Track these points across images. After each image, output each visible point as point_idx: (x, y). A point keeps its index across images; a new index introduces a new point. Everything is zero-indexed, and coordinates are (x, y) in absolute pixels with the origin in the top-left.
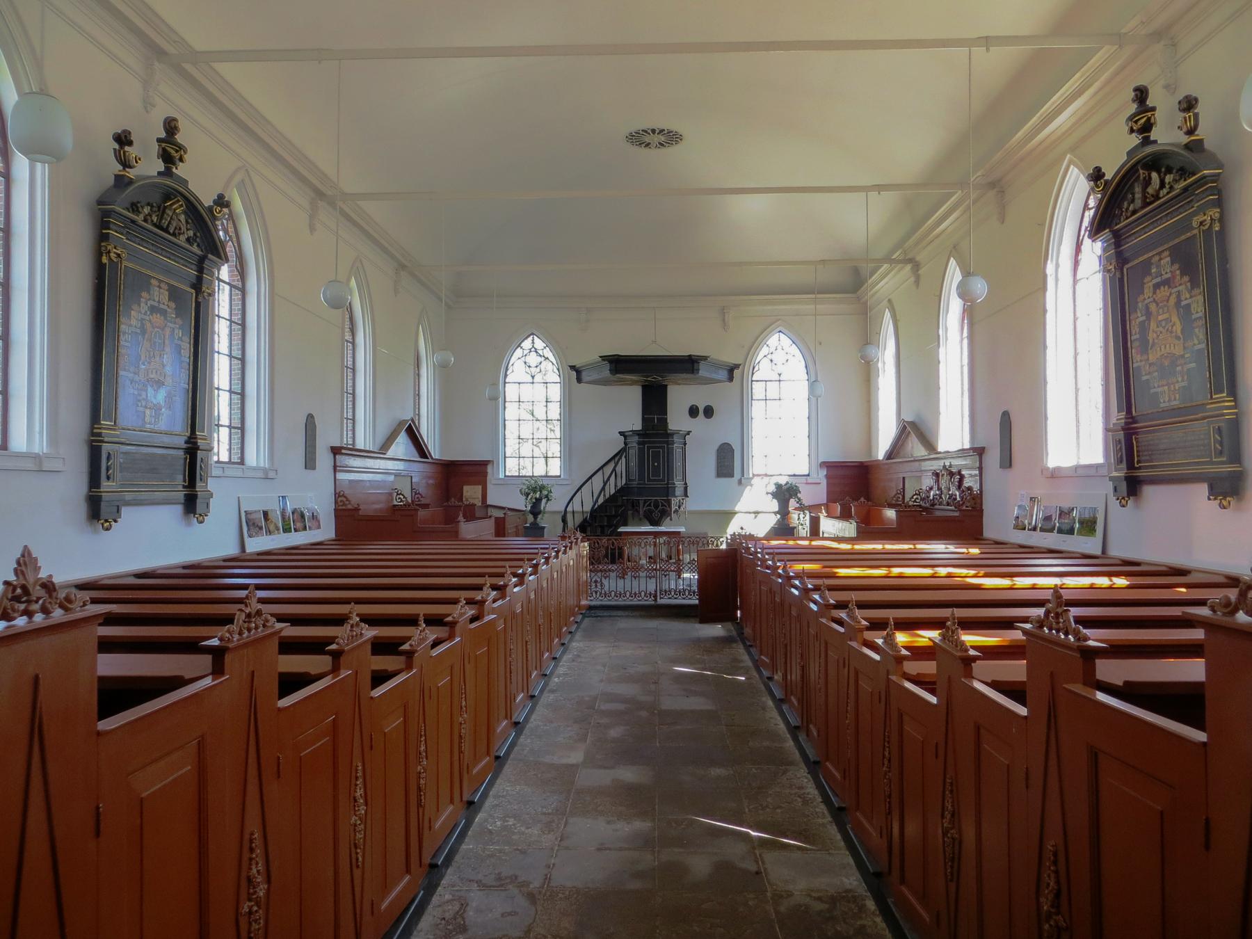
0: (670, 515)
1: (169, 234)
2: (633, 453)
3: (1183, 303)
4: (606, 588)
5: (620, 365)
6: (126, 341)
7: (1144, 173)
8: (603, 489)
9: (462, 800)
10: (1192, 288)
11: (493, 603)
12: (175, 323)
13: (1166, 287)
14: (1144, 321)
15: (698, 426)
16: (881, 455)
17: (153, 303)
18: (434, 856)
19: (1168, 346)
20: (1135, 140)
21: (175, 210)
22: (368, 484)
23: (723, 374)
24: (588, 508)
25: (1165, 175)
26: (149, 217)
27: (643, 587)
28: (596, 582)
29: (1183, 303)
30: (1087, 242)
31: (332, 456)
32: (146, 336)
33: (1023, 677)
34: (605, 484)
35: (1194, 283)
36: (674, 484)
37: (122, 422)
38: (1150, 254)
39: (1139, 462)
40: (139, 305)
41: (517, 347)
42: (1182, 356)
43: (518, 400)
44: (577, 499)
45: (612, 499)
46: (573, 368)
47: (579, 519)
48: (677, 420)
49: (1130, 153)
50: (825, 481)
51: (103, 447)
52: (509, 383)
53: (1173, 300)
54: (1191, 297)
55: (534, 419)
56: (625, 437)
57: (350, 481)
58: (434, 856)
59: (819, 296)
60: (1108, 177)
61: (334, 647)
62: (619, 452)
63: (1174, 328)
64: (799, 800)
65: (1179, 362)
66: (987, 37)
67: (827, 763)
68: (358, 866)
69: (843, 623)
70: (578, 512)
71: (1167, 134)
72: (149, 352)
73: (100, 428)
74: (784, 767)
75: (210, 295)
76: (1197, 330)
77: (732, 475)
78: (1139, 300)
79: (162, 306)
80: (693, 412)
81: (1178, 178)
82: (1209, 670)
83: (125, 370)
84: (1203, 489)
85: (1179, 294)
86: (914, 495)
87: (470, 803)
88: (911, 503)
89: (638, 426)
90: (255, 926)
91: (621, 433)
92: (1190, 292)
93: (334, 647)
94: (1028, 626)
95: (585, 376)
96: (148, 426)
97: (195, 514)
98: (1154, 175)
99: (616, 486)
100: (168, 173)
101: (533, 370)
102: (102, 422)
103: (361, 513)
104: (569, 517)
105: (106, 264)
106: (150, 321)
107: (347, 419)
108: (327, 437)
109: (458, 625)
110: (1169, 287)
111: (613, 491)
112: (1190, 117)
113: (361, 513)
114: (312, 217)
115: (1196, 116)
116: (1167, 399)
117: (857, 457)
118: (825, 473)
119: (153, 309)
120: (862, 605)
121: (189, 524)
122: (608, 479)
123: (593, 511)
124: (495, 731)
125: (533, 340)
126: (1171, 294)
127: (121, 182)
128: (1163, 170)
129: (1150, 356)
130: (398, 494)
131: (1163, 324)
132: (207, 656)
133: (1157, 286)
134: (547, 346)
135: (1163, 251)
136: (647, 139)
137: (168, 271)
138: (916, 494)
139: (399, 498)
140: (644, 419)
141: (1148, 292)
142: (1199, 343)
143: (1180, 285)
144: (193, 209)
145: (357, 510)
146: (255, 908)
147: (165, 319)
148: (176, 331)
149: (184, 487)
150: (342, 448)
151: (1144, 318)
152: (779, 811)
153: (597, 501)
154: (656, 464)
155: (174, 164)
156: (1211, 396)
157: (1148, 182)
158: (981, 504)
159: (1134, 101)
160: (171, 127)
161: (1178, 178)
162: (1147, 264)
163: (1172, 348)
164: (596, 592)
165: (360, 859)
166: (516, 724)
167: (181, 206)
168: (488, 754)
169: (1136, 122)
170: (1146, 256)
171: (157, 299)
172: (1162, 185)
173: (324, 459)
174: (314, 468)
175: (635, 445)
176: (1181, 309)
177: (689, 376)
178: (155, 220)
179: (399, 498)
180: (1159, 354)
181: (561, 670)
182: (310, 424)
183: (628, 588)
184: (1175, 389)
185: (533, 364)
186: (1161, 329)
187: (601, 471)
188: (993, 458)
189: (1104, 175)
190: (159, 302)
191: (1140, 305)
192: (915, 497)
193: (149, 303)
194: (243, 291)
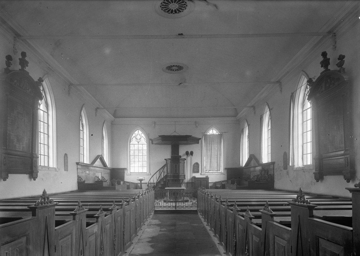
2: (169, 165)
4: (161, 205)
5: (165, 139)
8: (160, 176)
16: (244, 165)
20: (323, 69)
24: (155, 181)
28: (157, 203)
30: (306, 101)
33: (261, 222)
34: (160, 175)
45: (162, 179)
55: (138, 134)
56: (166, 160)
62: (164, 165)
70: (152, 183)
82: (292, 218)
91: (165, 159)
94: (261, 210)
95: (154, 142)
96: (17, 149)
101: (138, 140)
103: (85, 183)
111: (163, 177)
113: (85, 183)
120: (251, 211)
122: (161, 173)
123: (157, 183)
125: (138, 132)
132: (264, 163)
138: (254, 177)
145: (84, 182)
153: (158, 180)
164: (194, 206)
173: (72, 166)
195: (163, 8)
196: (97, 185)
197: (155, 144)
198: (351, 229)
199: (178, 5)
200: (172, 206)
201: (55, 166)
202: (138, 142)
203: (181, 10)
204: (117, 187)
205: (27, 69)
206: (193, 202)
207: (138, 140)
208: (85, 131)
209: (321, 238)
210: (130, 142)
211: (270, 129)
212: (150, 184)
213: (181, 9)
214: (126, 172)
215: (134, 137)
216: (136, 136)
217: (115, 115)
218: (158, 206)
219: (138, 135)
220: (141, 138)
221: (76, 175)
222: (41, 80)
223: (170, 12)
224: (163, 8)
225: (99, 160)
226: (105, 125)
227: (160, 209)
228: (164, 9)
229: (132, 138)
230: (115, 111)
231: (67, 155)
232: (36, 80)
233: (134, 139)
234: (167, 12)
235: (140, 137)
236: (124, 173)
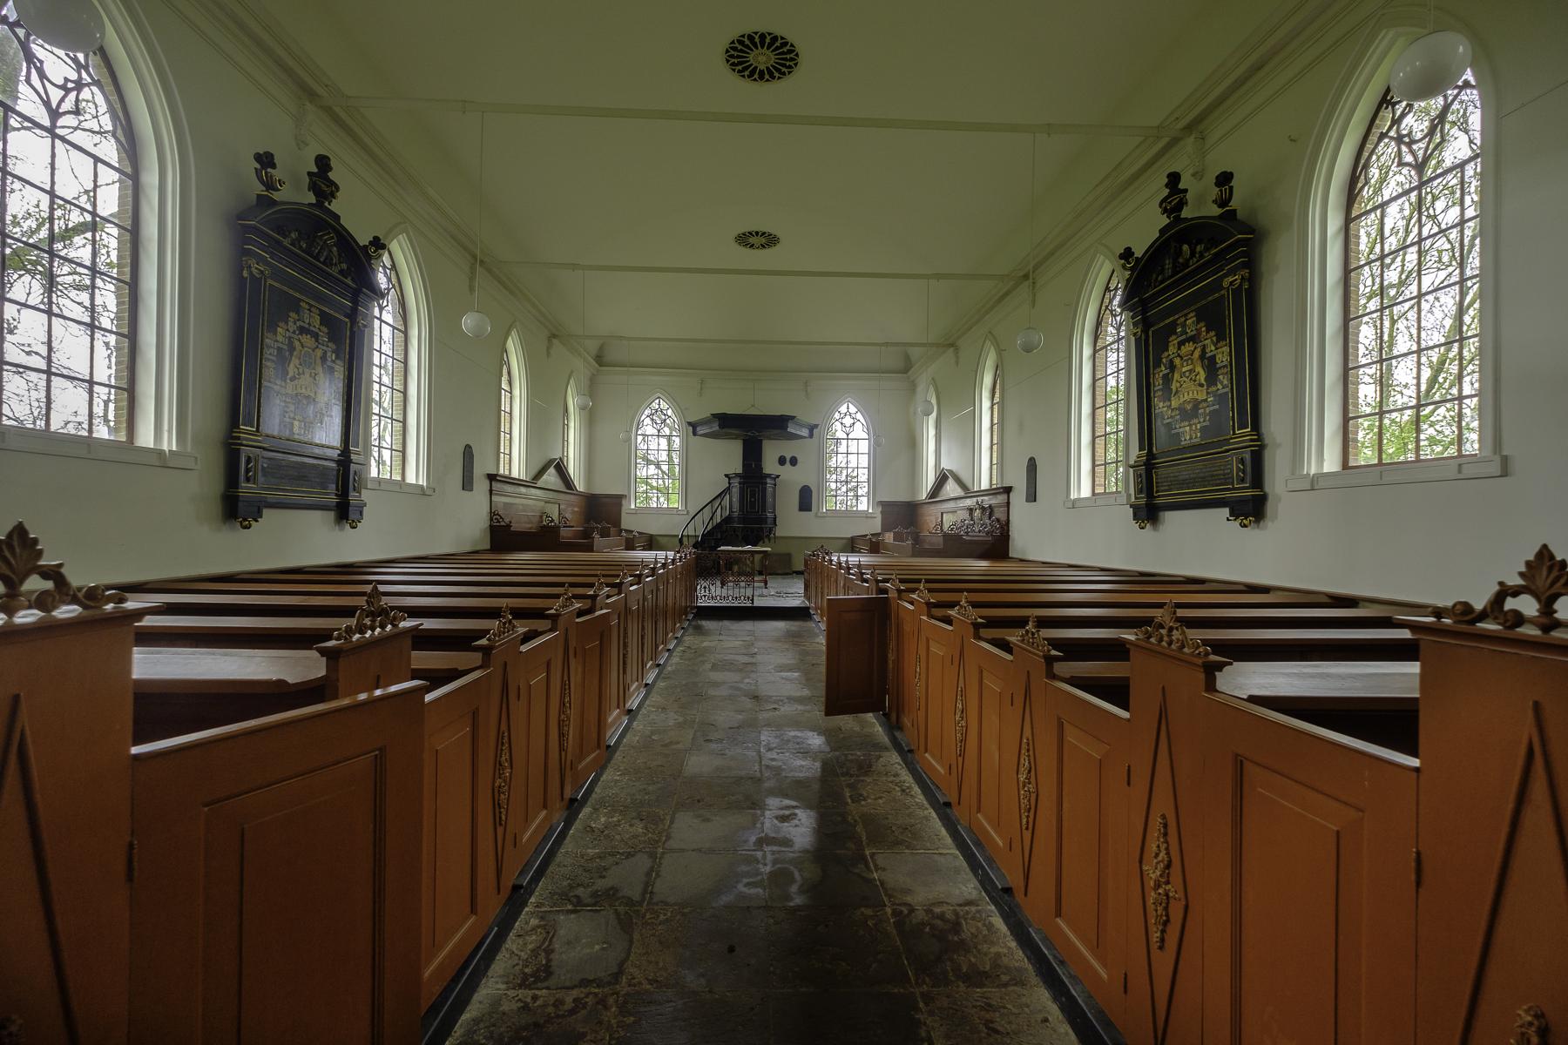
0: (763, 539)
1: (320, 262)
2: (735, 491)
3: (1207, 355)
5: (727, 424)
6: (270, 354)
7: (1175, 246)
8: (712, 518)
9: (562, 799)
10: (1218, 341)
11: (607, 598)
12: (328, 346)
13: (1191, 343)
14: (1168, 374)
15: (786, 472)
17: (302, 324)
18: (522, 873)
19: (1191, 392)
21: (326, 240)
22: (521, 507)
23: (805, 432)
24: (700, 533)
25: (1196, 245)
26: (296, 243)
27: (743, 590)
29: (1207, 355)
31: (488, 482)
32: (295, 353)
35: (1221, 337)
37: (265, 429)
38: (1177, 317)
39: (1157, 492)
40: (287, 323)
42: (1206, 400)
45: (718, 526)
46: (690, 424)
47: (692, 541)
48: (770, 465)
49: (1162, 231)
50: (880, 516)
51: (241, 451)
53: (1197, 354)
54: (1217, 349)
56: (729, 479)
57: (505, 504)
58: (522, 873)
59: (882, 375)
60: (1138, 253)
61: (484, 642)
62: (722, 492)
63: (1198, 377)
64: (897, 789)
65: (1201, 406)
66: (1049, 125)
67: (926, 755)
68: (501, 824)
69: (952, 621)
70: (692, 536)
71: (1201, 205)
72: (298, 369)
73: (240, 432)
74: (877, 753)
75: (365, 326)
76: (1221, 377)
77: (810, 510)
78: (1163, 356)
79: (312, 328)
80: (782, 461)
81: (1209, 246)
83: (270, 382)
84: (1226, 511)
85: (1204, 347)
87: (573, 801)
89: (740, 470)
90: (502, 796)
91: (726, 476)
92: (1215, 345)
93: (484, 642)
96: (296, 437)
97: (347, 520)
98: (1185, 247)
99: (721, 516)
100: (319, 205)
102: (242, 427)
103: (512, 529)
105: (247, 278)
106: (299, 340)
107: (504, 453)
108: (481, 469)
109: (560, 618)
110: (1194, 343)
111: (719, 521)
112: (1226, 189)
113: (512, 529)
114: (472, 279)
115: (1231, 188)
116: (1188, 438)
117: (902, 497)
119: (302, 330)
121: (342, 529)
124: (606, 720)
126: (1195, 348)
127: (264, 202)
128: (1194, 241)
129: (1173, 402)
131: (1187, 374)
133: (1181, 344)
135: (1189, 313)
136: (752, 240)
137: (319, 298)
141: (1172, 349)
142: (1223, 388)
143: (1206, 339)
144: (345, 240)
145: (509, 526)
146: (503, 784)
147: (317, 341)
148: (329, 354)
149: (336, 495)
150: (496, 475)
151: (1168, 371)
152: (880, 801)
155: (326, 199)
156: (1234, 434)
157: (1179, 253)
158: (1008, 530)
159: (1167, 186)
160: (323, 163)
161: (1209, 246)
162: (1174, 324)
163: (1195, 395)
165: (503, 818)
166: (630, 711)
167: (332, 238)
168: (599, 746)
169: (1170, 203)
170: (1171, 319)
171: (307, 321)
172: (1193, 254)
173: (481, 485)
174: (471, 490)
176: (1206, 361)
177: (778, 431)
178: (304, 246)
180: (1182, 400)
181: (675, 660)
182: (468, 453)
184: (1196, 429)
186: (1184, 379)
188: (1018, 498)
189: (1133, 253)
190: (309, 324)
191: (1164, 360)
193: (298, 323)
194: (406, 333)
195: (732, 56)
196: (544, 537)
197: (705, 435)
198: (1415, 762)
199: (773, 57)
201: (423, 482)
202: (848, 435)
203: (784, 69)
204: (598, 540)
205: (335, 206)
208: (516, 392)
209: (1252, 761)
211: (998, 403)
212: (685, 539)
213: (779, 71)
214: (624, 502)
215: (648, 416)
217: (600, 359)
218: (705, 596)
219: (848, 417)
220: (854, 424)
221: (486, 509)
222: (378, 244)
223: (747, 73)
224: (732, 56)
225: (552, 470)
226: (572, 381)
227: (712, 604)
228: (733, 60)
230: (601, 348)
231: (470, 447)
232: (363, 239)
233: (648, 421)
234: (739, 71)
235: (852, 421)
236: (620, 505)
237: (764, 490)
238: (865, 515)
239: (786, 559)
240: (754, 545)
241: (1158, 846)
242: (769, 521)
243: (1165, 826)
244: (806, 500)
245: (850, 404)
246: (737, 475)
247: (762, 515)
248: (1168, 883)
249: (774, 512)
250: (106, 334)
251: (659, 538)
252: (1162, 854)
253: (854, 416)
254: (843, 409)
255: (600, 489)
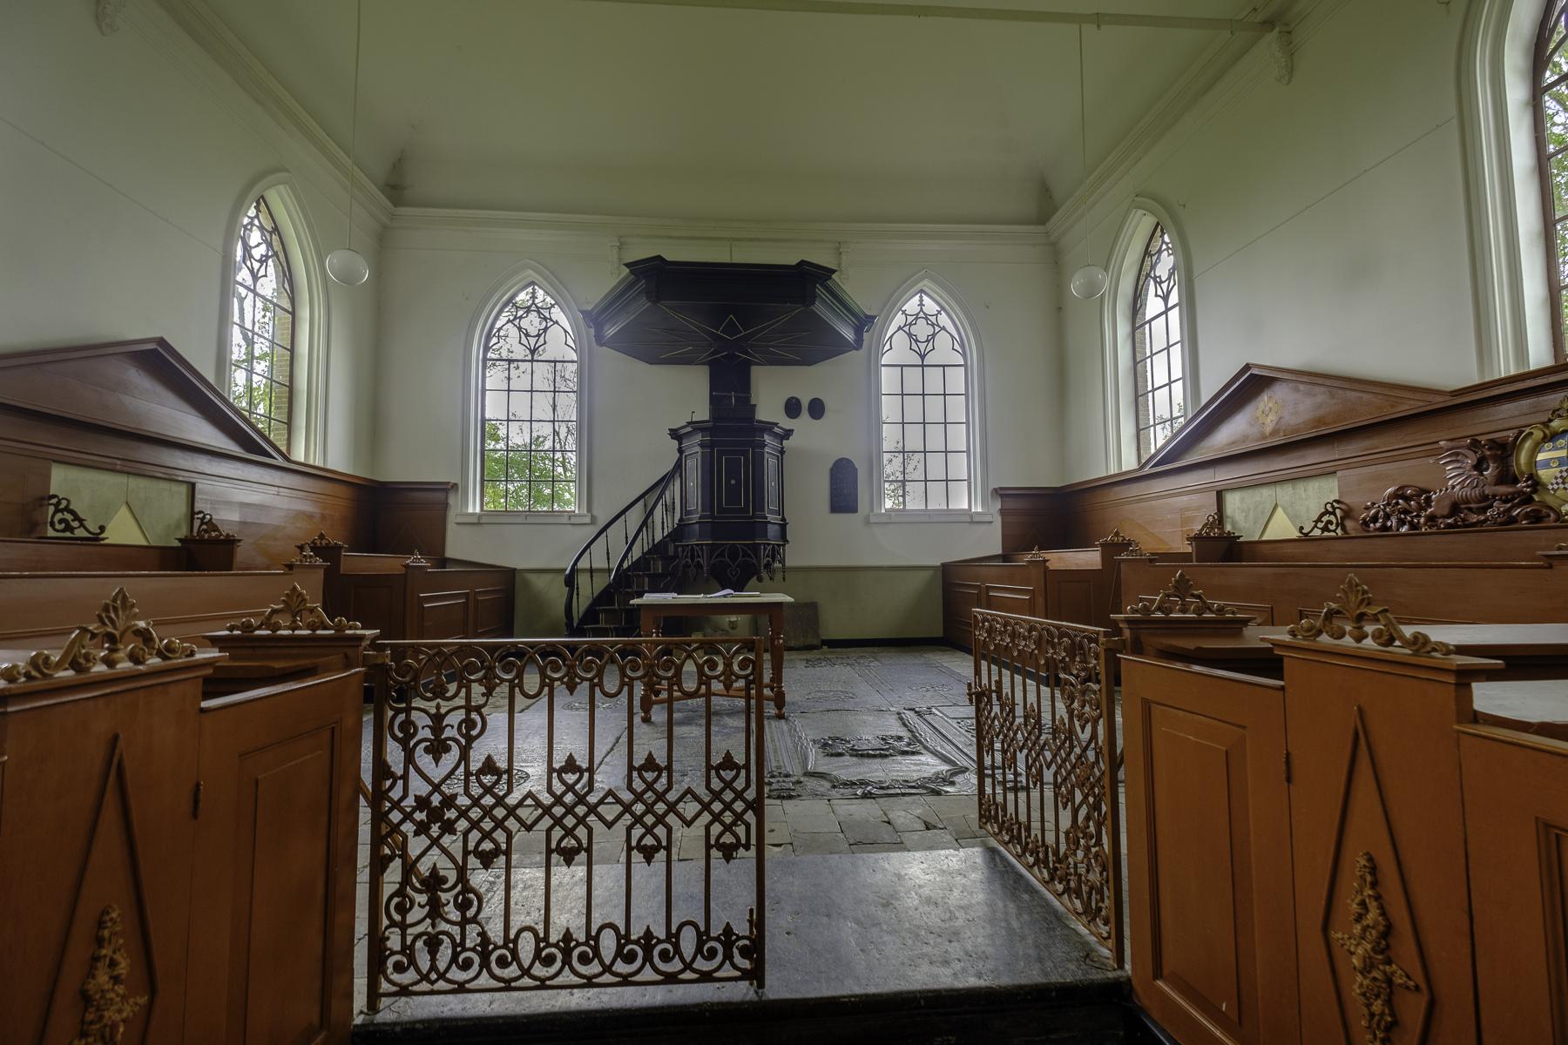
2: (693, 466)
15: (803, 426)
36: (766, 518)
41: (506, 305)
43: (507, 388)
44: (599, 547)
50: (999, 518)
52: (549, 421)
55: (921, 315)
77: (854, 510)
80: (792, 408)
86: (1322, 515)
88: (1317, 532)
89: (703, 413)
101: (532, 341)
104: (583, 581)
111: (659, 537)
117: (1045, 477)
118: (1000, 507)
130: (57, 511)
134: (556, 303)
138: (1327, 512)
139: (61, 521)
140: (713, 400)
154: (733, 482)
164: (433, 944)
175: (698, 449)
179: (61, 521)
183: (608, 910)
185: (533, 332)
187: (643, 500)
192: (1325, 519)
200: (702, 937)
202: (923, 357)
206: (424, 868)
207: (532, 341)
210: (487, 349)
215: (900, 328)
216: (910, 324)
219: (922, 322)
220: (934, 335)
229: (891, 337)
235: (930, 330)
236: (445, 506)
237: (759, 461)
238: (969, 519)
239: (807, 613)
240: (739, 587)
241: (1363, 904)
242: (772, 531)
243: (1373, 870)
244: (843, 497)
245: (925, 297)
246: (696, 426)
247: (754, 516)
248: (1389, 962)
249: (781, 511)
250: (1534, 410)
251: (532, 578)
252: (1373, 915)
253: (933, 319)
254: (912, 306)
255: (398, 469)
